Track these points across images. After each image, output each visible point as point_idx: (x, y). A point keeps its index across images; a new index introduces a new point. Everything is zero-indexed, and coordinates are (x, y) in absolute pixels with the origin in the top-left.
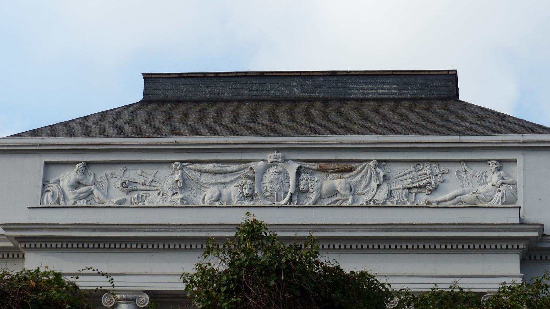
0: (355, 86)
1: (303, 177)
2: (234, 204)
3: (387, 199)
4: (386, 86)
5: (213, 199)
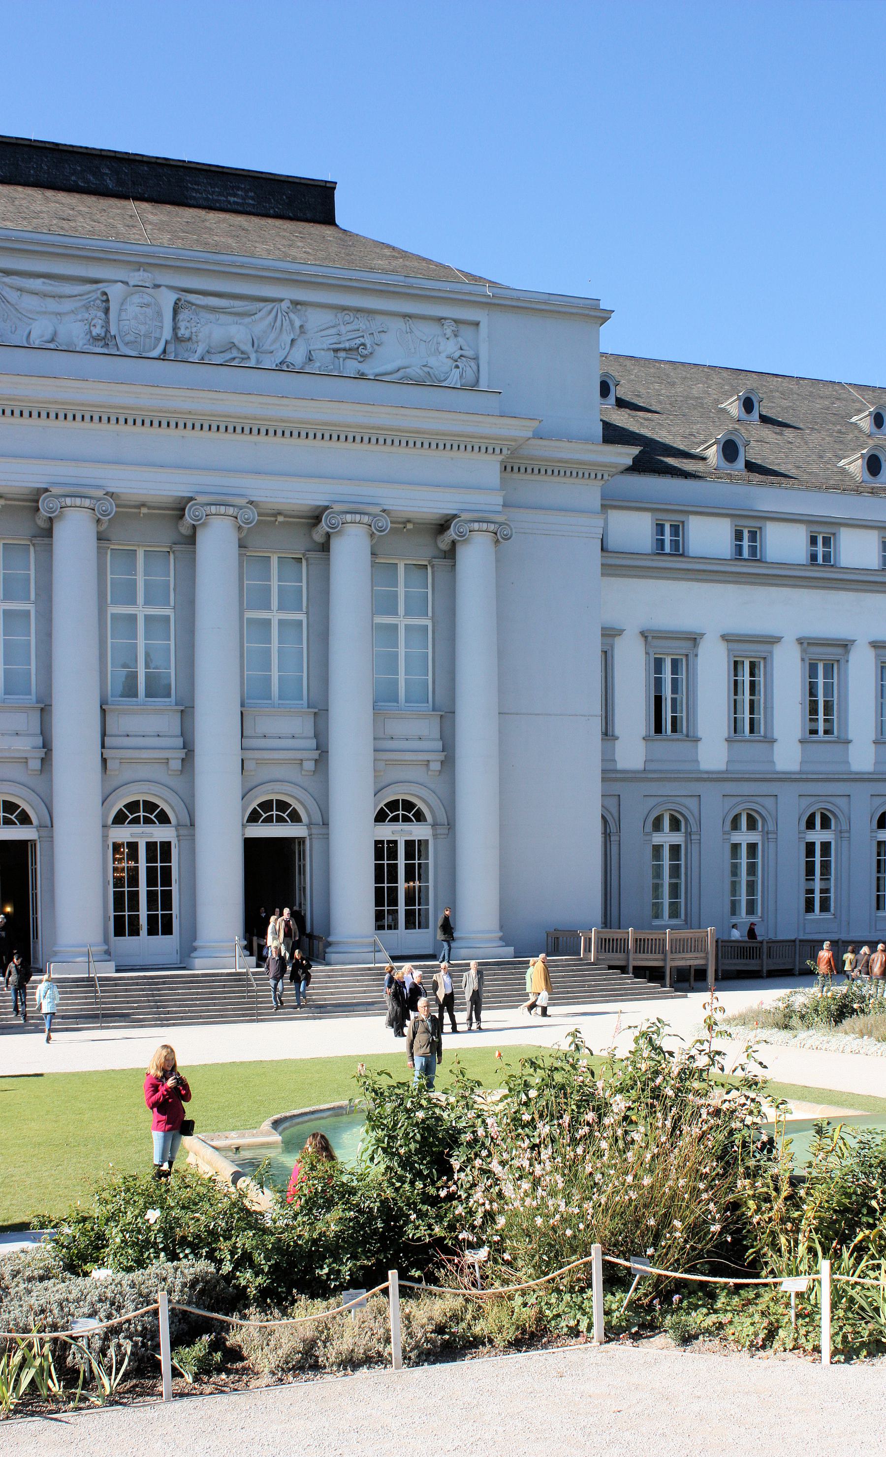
0: (196, 187)
1: (183, 315)
2: (78, 349)
3: (306, 363)
4: (240, 193)
5: (45, 339)
